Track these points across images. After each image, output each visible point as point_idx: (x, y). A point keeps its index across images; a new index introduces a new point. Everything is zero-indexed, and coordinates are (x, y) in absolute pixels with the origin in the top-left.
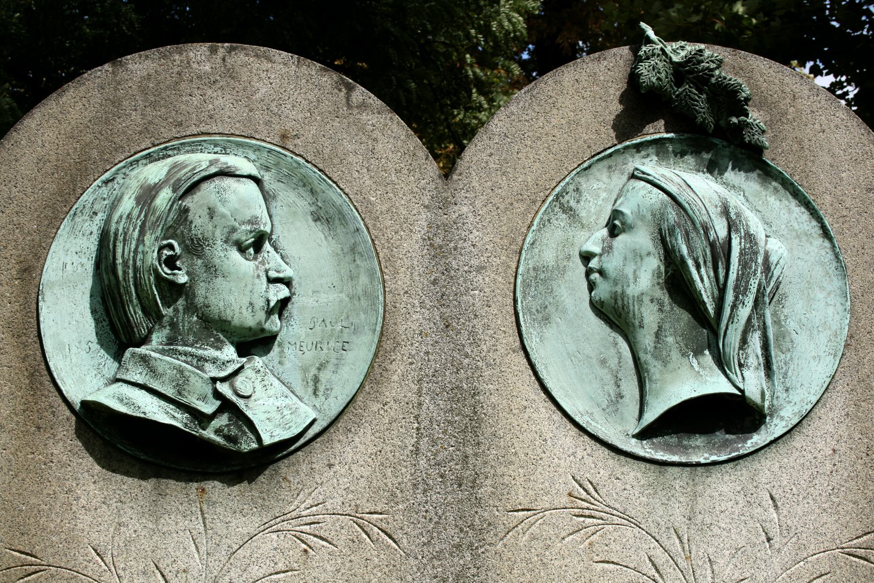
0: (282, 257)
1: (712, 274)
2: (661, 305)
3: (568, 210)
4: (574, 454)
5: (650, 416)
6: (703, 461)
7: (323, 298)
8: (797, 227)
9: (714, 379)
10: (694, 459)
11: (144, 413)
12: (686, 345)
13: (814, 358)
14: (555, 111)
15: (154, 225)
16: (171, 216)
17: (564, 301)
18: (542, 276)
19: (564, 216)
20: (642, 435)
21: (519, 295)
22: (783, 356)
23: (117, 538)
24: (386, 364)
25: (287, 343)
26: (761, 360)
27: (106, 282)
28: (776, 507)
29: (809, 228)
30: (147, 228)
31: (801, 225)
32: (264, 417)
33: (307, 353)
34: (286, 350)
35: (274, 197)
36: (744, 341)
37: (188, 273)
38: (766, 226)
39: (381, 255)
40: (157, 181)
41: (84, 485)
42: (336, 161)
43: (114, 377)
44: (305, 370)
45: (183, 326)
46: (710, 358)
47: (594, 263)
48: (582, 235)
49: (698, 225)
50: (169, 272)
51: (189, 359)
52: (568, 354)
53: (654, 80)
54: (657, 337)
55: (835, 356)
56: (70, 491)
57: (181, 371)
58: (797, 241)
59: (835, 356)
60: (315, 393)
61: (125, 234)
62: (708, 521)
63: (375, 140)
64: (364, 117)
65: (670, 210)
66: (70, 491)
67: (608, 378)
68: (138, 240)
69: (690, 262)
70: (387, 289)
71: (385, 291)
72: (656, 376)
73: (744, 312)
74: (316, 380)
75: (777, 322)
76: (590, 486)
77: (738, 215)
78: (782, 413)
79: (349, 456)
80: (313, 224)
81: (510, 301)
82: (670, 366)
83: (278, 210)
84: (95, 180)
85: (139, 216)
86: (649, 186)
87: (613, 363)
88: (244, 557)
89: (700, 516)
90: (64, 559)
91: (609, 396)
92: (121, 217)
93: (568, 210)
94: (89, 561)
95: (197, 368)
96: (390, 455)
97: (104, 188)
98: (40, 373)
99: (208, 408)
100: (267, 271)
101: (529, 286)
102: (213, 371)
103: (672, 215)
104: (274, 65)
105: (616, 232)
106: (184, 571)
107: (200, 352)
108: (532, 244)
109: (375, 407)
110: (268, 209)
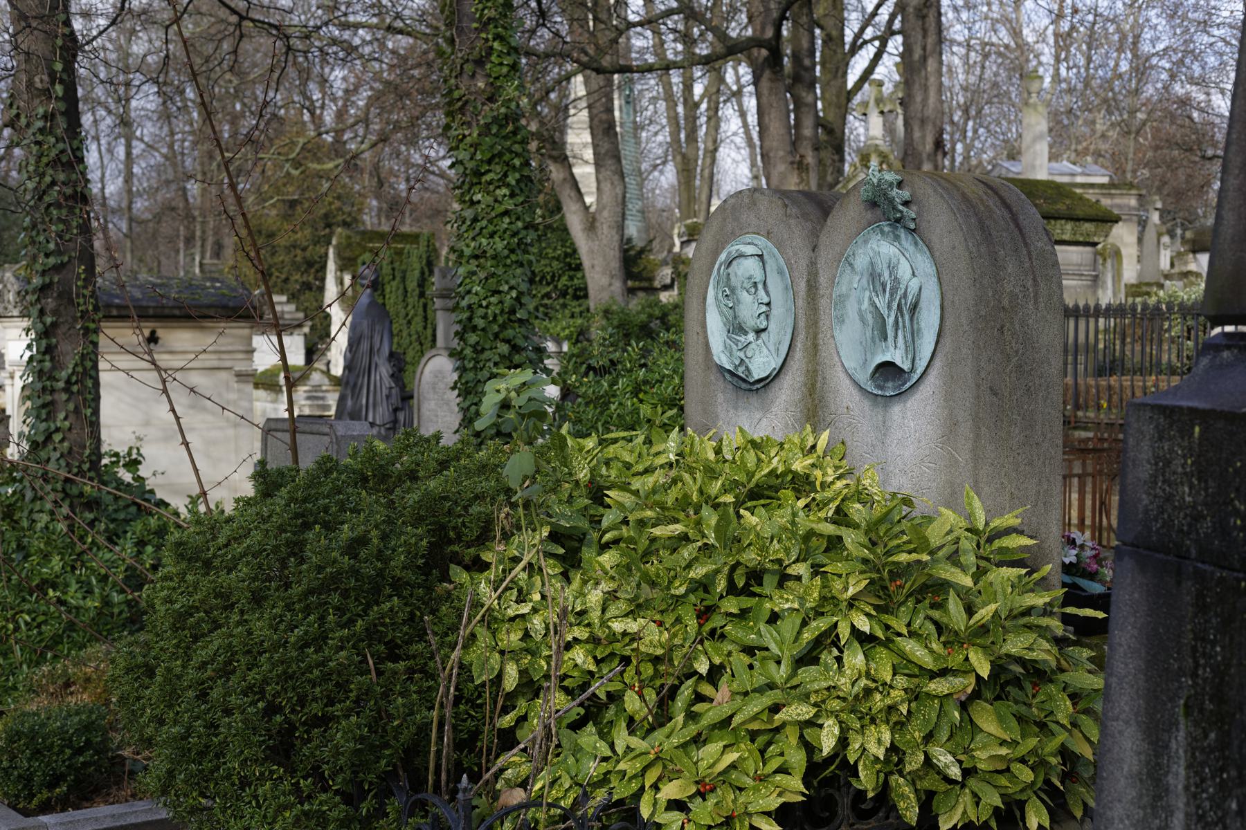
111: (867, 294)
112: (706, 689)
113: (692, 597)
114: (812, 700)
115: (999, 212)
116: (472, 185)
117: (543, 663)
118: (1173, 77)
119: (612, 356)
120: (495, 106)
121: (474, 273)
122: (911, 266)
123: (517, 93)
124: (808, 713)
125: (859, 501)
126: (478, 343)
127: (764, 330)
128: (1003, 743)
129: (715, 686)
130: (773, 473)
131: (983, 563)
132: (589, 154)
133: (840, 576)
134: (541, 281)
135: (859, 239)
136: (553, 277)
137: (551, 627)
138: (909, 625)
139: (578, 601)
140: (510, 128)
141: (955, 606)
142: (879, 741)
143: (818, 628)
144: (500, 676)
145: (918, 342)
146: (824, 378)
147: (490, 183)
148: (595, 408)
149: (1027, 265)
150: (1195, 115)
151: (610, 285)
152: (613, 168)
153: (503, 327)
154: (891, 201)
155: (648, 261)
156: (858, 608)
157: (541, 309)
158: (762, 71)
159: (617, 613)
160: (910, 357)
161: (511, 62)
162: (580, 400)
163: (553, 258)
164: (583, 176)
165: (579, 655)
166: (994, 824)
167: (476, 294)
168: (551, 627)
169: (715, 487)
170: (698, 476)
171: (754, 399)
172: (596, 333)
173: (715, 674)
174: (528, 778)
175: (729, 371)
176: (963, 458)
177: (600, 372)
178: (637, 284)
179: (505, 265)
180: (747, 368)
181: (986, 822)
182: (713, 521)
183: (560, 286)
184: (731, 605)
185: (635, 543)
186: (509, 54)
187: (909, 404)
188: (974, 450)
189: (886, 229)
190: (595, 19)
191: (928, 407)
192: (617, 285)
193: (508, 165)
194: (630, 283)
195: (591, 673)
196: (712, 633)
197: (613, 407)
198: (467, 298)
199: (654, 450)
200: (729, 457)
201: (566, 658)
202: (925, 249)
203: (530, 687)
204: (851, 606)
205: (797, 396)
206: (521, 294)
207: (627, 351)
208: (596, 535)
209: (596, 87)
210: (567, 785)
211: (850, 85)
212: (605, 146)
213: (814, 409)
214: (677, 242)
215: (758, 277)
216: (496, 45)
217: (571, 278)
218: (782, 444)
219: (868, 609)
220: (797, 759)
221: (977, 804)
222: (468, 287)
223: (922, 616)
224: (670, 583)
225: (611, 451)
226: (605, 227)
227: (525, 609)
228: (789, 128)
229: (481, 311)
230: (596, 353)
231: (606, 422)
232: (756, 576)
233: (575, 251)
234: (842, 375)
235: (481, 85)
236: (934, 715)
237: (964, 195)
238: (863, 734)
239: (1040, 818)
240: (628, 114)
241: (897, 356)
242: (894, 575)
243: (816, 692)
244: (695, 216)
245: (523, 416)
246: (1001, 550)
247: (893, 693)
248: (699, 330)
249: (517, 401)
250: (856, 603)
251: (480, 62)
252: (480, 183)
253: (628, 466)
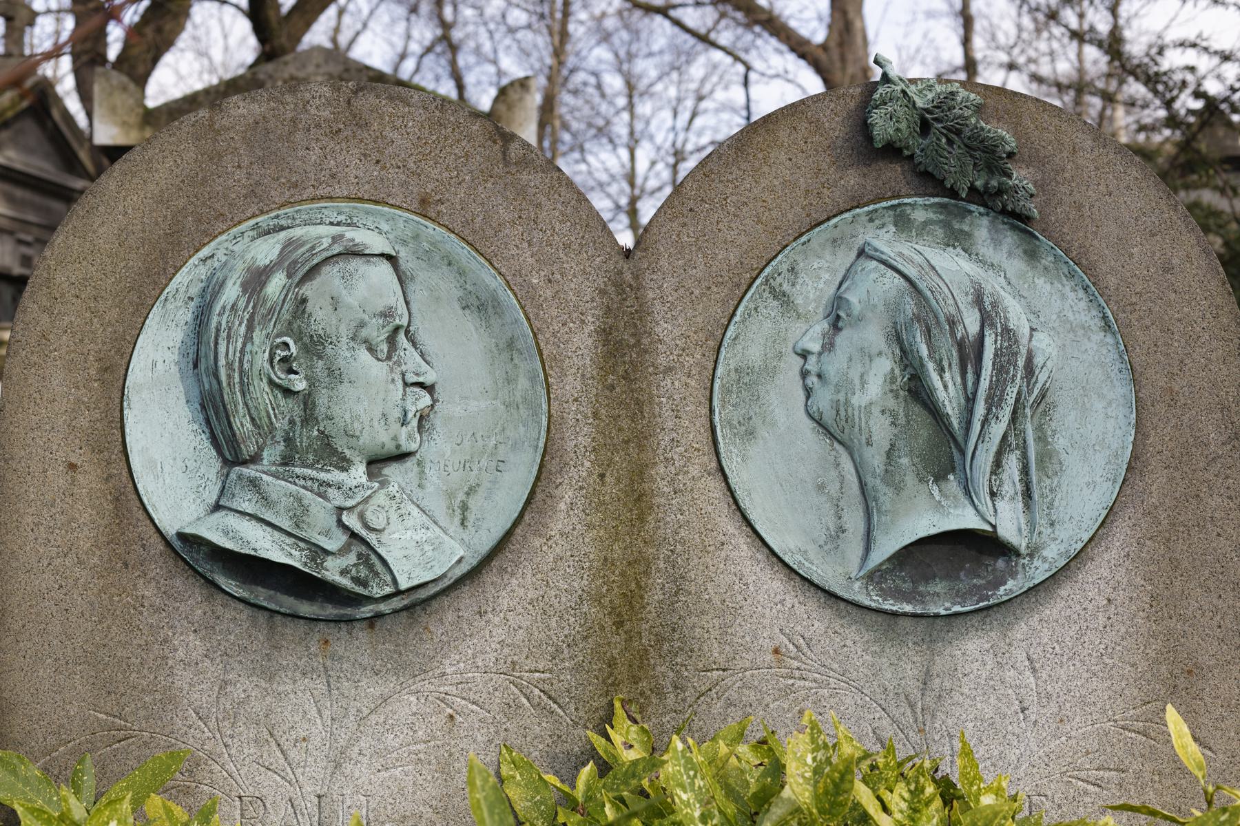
0: (422, 355)
1: (959, 380)
2: (894, 416)
3: (780, 296)
4: (782, 602)
5: (887, 546)
6: (943, 612)
7: (474, 406)
8: (1071, 318)
9: (959, 511)
10: (933, 610)
11: (255, 550)
12: (925, 468)
13: (1088, 484)
14: (766, 169)
15: (266, 318)
16: (286, 307)
17: (773, 411)
18: (746, 380)
19: (775, 303)
20: (874, 577)
21: (716, 402)
22: (1048, 482)
23: (222, 700)
24: (551, 489)
25: (428, 461)
26: (1019, 488)
27: (207, 386)
28: (1034, 670)
29: (1088, 318)
30: (256, 322)
31: (1077, 316)
32: (400, 554)
33: (454, 474)
34: (427, 471)
35: (412, 279)
36: (998, 464)
37: (307, 378)
38: (1032, 317)
39: (545, 353)
40: (267, 262)
41: (182, 634)
42: (490, 232)
43: (217, 502)
44: (450, 495)
45: (301, 442)
46: (955, 484)
47: (812, 365)
48: (797, 328)
49: (942, 319)
50: (283, 376)
51: (309, 483)
52: (777, 477)
53: (891, 131)
54: (888, 457)
55: (1114, 482)
56: (165, 641)
57: (299, 500)
58: (1071, 335)
59: (1114, 482)
60: (463, 523)
61: (230, 329)
62: (947, 685)
63: (539, 205)
64: (524, 177)
65: (908, 299)
66: (165, 641)
67: (828, 509)
68: (245, 337)
69: (931, 366)
70: (552, 396)
71: (549, 398)
72: (887, 506)
73: (998, 429)
74: (464, 508)
75: (1041, 439)
76: (802, 641)
77: (994, 305)
78: (1045, 553)
79: (505, 603)
80: (460, 312)
81: (704, 411)
82: (904, 494)
83: (418, 294)
84: (190, 257)
85: (246, 307)
86: (883, 267)
87: (833, 488)
88: (377, 724)
89: (937, 680)
90: (159, 723)
91: (828, 529)
92: (224, 308)
93: (780, 296)
94: (190, 727)
95: (319, 495)
96: (555, 601)
97: (201, 267)
98: (125, 498)
99: (334, 542)
100: (403, 375)
101: (730, 392)
102: (337, 499)
103: (910, 307)
104: (412, 110)
105: (840, 324)
106: (304, 739)
107: (323, 476)
108: (735, 339)
109: (537, 542)
110: (404, 293)
187: (1020, 631)
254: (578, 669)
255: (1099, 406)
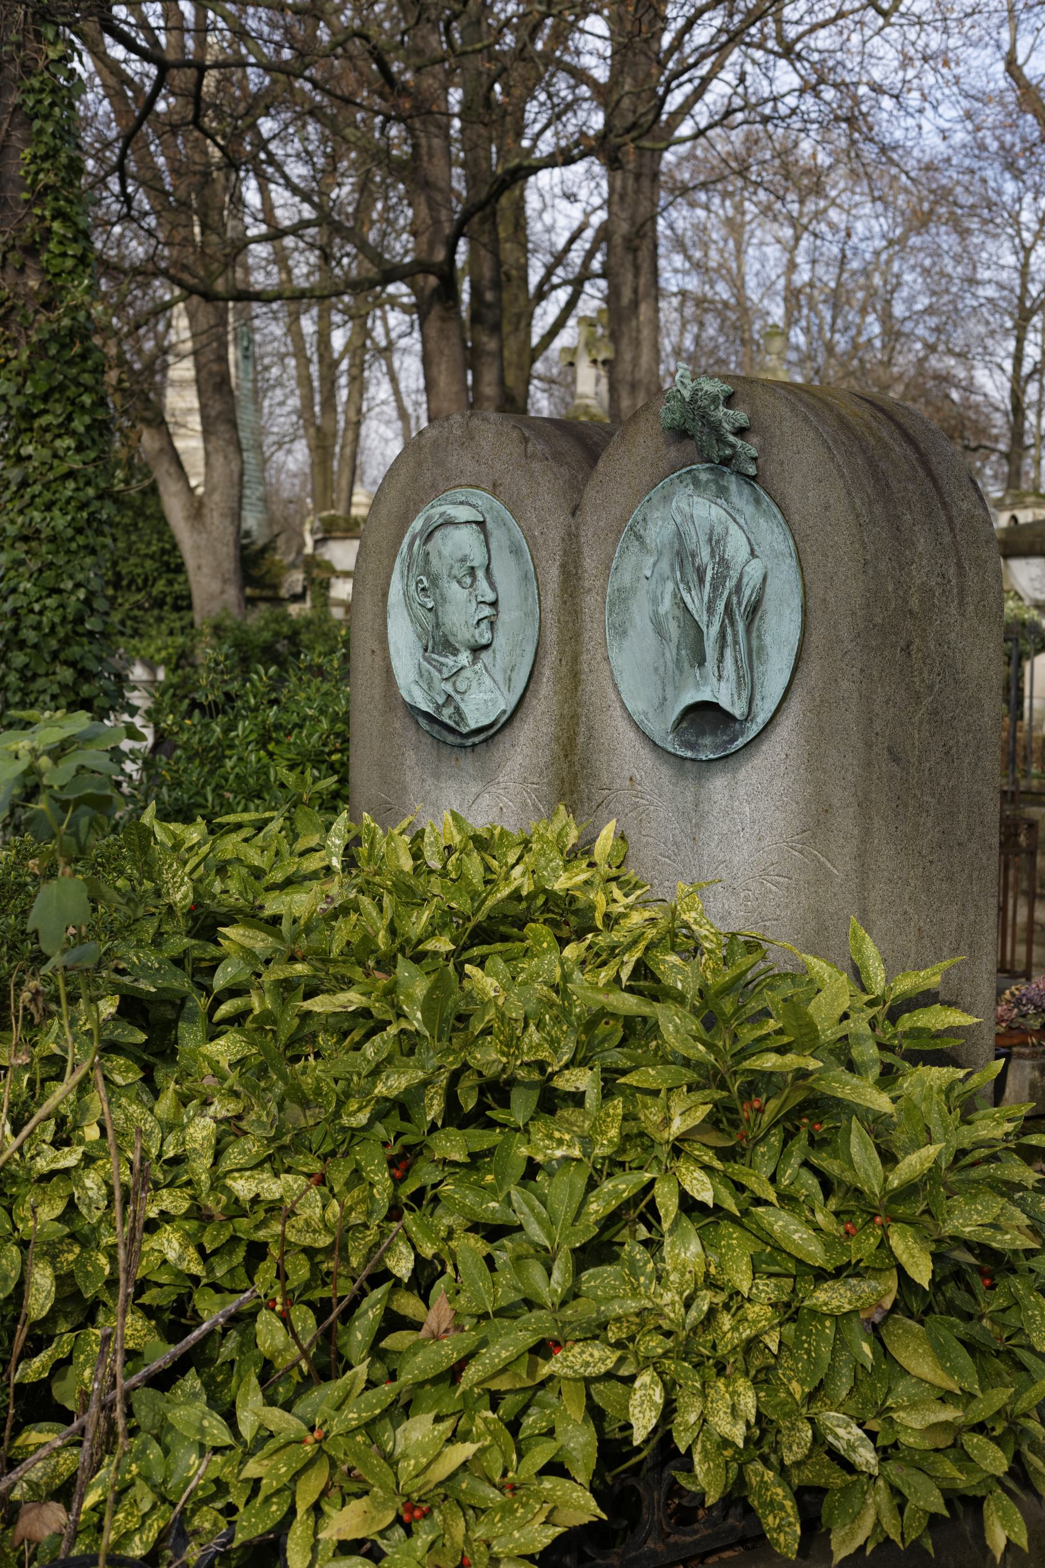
87: (662, 670)
107: (442, 659)
111: (670, 586)
112: (409, 1305)
113: (380, 1129)
114: (612, 1335)
115: (899, 449)
116: (19, 432)
117: (103, 1260)
118: (931, 348)
119: (227, 688)
120: (53, 316)
121: (21, 563)
122: (752, 541)
123: (87, 299)
124: (603, 1360)
125: (673, 948)
126: (26, 666)
127: (486, 647)
128: (945, 1398)
129: (425, 1298)
130: (516, 896)
131: (889, 1058)
132: (195, 422)
133: (656, 1093)
134: (129, 586)
135: (655, 494)
136: (146, 580)
137: (118, 1194)
138: (773, 1179)
139: (171, 1138)
140: (77, 349)
141: (860, 1148)
142: (734, 1410)
143: (616, 1193)
144: (21, 1285)
145: (759, 669)
146: (590, 728)
147: (46, 429)
148: (202, 764)
149: (947, 540)
150: (955, 395)
151: (222, 592)
152: (227, 436)
153: (65, 642)
154: (715, 428)
155: (273, 563)
156: (689, 1156)
157: (129, 623)
158: (430, 306)
159: (243, 1161)
160: (745, 694)
161: (79, 253)
162: (179, 752)
163: (146, 556)
164: (187, 451)
165: (170, 1244)
166: (928, 1544)
167: (25, 593)
168: (118, 1194)
169: (419, 921)
170: (387, 901)
171: (468, 762)
172: (206, 652)
173: (424, 1278)
174: (74, 1476)
175: (426, 715)
176: (841, 868)
177: (211, 710)
178: (257, 592)
179: (68, 552)
180: (458, 710)
181: (916, 1542)
182: (420, 988)
183: (154, 592)
184: (453, 1146)
185: (275, 1022)
186: (75, 240)
187: (742, 774)
188: (861, 856)
189: (704, 477)
190: (204, 227)
191: (778, 781)
192: (232, 593)
193: (73, 403)
194: (249, 591)
195: (195, 1279)
196: (418, 1197)
197: (229, 764)
198: (11, 599)
199: (301, 845)
200: (436, 864)
201: (145, 1248)
202: (776, 510)
203: (77, 1306)
204: (677, 1151)
205: (543, 758)
206: (91, 594)
207: (250, 680)
208: (202, 1003)
209: (205, 327)
210: (146, 1506)
211: (535, 340)
212: (216, 407)
213: (573, 779)
214: (309, 540)
215: (478, 558)
216: (56, 226)
217: (170, 583)
218: (526, 844)
219: (708, 1157)
220: (579, 1442)
221: (901, 1508)
222: (12, 584)
223: (795, 1161)
224: (341, 1104)
225: (230, 845)
226: (215, 514)
227: (70, 1158)
228: (466, 389)
229: (32, 619)
230: (203, 682)
231: (218, 787)
232: (498, 1090)
233: (175, 547)
234: (623, 725)
235: (33, 284)
236: (825, 1350)
237: (840, 418)
238: (705, 1396)
239: (1011, 1529)
240: (246, 373)
241: (724, 694)
242: (750, 1090)
243: (618, 1319)
244: (333, 507)
245: (64, 805)
246: (916, 1033)
247: (753, 1311)
248: (375, 646)
249: (56, 776)
250: (686, 1147)
251: (32, 250)
252: (31, 430)
253: (257, 873)
254: (549, 784)
255: (787, 612)
